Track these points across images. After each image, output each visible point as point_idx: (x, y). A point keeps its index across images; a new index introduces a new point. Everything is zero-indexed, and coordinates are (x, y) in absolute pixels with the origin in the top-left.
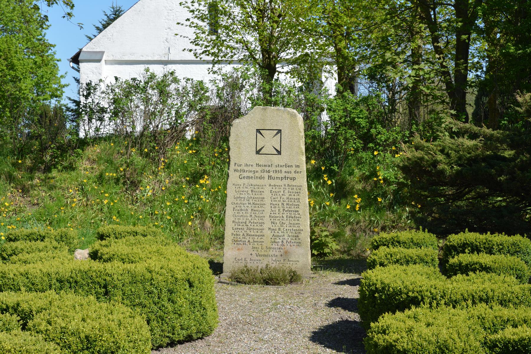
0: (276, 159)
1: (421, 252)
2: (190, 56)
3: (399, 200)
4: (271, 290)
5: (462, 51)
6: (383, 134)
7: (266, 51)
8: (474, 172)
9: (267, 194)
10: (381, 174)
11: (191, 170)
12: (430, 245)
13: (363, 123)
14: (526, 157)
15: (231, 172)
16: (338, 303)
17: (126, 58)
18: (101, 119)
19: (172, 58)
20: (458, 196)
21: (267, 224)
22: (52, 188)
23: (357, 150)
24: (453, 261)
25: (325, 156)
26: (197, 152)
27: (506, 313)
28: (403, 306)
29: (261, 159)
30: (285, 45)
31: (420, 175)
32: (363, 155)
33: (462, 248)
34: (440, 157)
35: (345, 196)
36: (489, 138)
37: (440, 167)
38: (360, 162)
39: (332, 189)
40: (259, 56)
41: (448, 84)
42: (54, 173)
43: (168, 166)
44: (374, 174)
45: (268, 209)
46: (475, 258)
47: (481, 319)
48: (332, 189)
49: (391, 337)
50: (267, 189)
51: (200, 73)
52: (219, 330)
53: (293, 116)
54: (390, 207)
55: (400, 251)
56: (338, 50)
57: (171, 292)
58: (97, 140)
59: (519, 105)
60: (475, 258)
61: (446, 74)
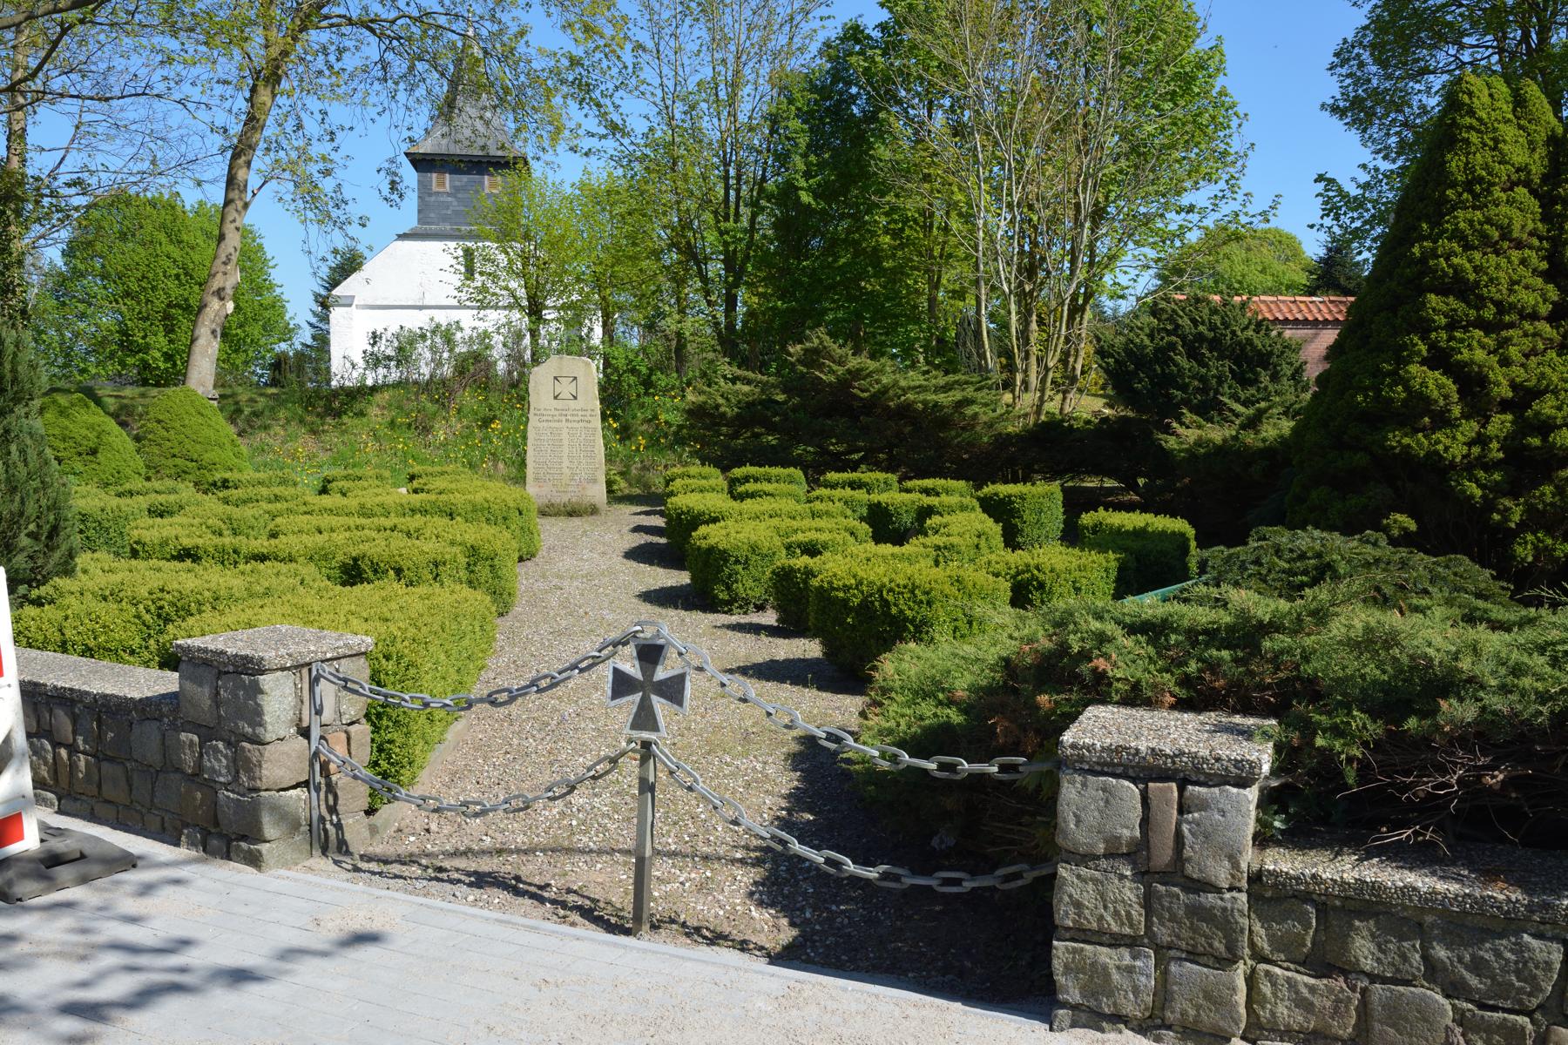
0: (572, 404)
1: (712, 482)
2: (455, 302)
3: (680, 440)
4: (576, 521)
5: (731, 302)
6: (661, 379)
7: (532, 299)
8: (753, 414)
9: (565, 436)
10: (663, 417)
11: (481, 415)
12: (717, 478)
13: (644, 370)
14: (796, 400)
15: (531, 416)
16: (638, 529)
17: (378, 303)
18: (387, 367)
19: (427, 303)
20: (736, 436)
21: (566, 463)
22: (344, 432)
23: (638, 396)
24: (741, 489)
25: (612, 399)
26: (486, 399)
27: (795, 524)
28: (715, 520)
29: (558, 404)
30: (551, 293)
31: (700, 415)
32: (647, 400)
33: (746, 479)
34: (721, 401)
35: (629, 438)
36: (765, 384)
37: (722, 409)
38: (642, 406)
39: (616, 431)
40: (525, 303)
41: (720, 334)
42: (345, 419)
43: (459, 411)
44: (655, 417)
45: (566, 450)
46: (758, 486)
47: (777, 529)
48: (616, 431)
49: (712, 541)
50: (565, 431)
51: (468, 321)
52: (542, 553)
53: (588, 364)
54: (671, 447)
55: (694, 483)
56: (604, 299)
57: (505, 519)
58: (385, 386)
59: (790, 355)
60: (758, 486)
61: (717, 324)
